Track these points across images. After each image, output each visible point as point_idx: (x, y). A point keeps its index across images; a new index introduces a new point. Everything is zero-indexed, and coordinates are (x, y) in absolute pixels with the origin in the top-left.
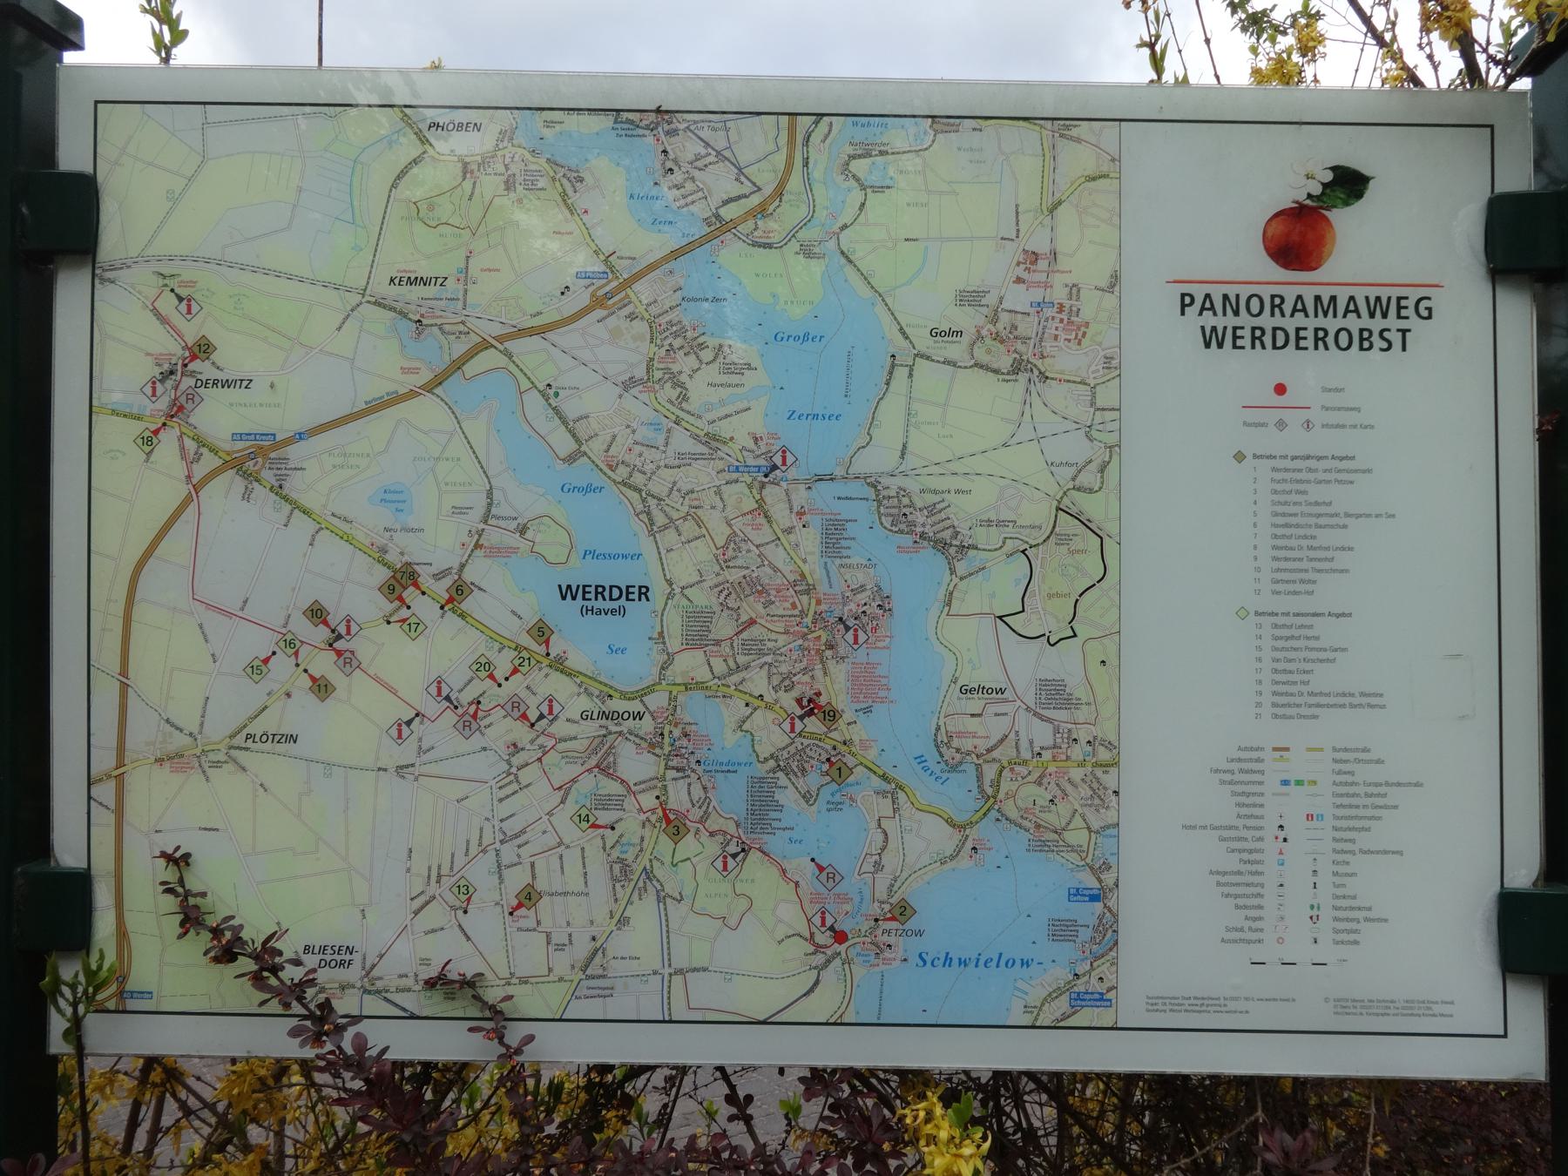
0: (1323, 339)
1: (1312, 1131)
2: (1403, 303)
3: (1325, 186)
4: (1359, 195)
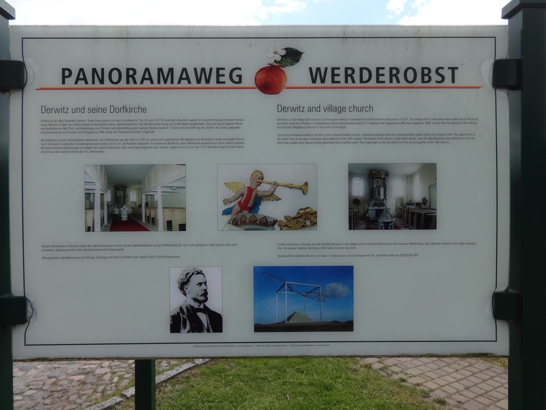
1: (124, 375)
2: (221, 72)
4: (297, 61)
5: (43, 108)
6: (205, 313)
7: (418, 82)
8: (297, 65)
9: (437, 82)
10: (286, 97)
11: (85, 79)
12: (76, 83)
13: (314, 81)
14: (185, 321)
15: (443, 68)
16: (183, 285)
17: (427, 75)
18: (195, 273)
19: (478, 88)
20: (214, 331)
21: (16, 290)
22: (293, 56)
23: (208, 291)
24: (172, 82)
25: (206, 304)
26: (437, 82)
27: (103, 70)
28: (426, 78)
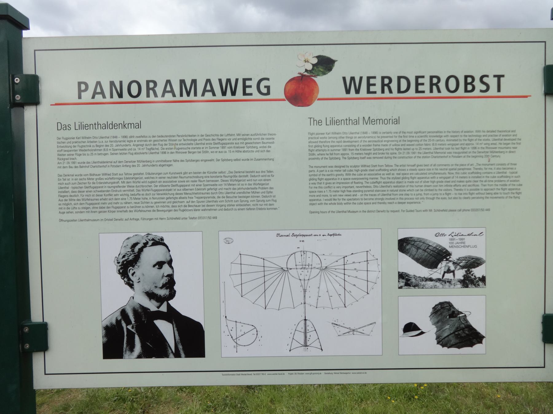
0: (436, 84)
3: (314, 65)
4: (330, 69)
5: (59, 124)
6: (169, 321)
7: (461, 92)
8: (330, 74)
9: (481, 91)
10: (316, 109)
11: (102, 93)
12: (93, 97)
13: (348, 91)
14: (131, 336)
15: (487, 76)
16: (126, 267)
17: (471, 83)
18: (150, 243)
19: (526, 97)
20: (189, 355)
21: (36, 317)
22: (325, 64)
23: (175, 278)
24: (195, 95)
25: (172, 302)
26: (481, 91)
27: (121, 83)
28: (470, 87)
